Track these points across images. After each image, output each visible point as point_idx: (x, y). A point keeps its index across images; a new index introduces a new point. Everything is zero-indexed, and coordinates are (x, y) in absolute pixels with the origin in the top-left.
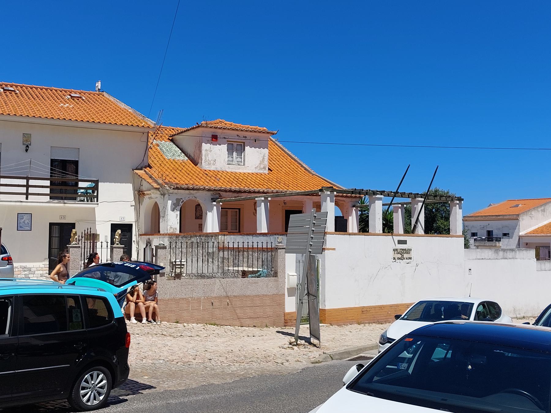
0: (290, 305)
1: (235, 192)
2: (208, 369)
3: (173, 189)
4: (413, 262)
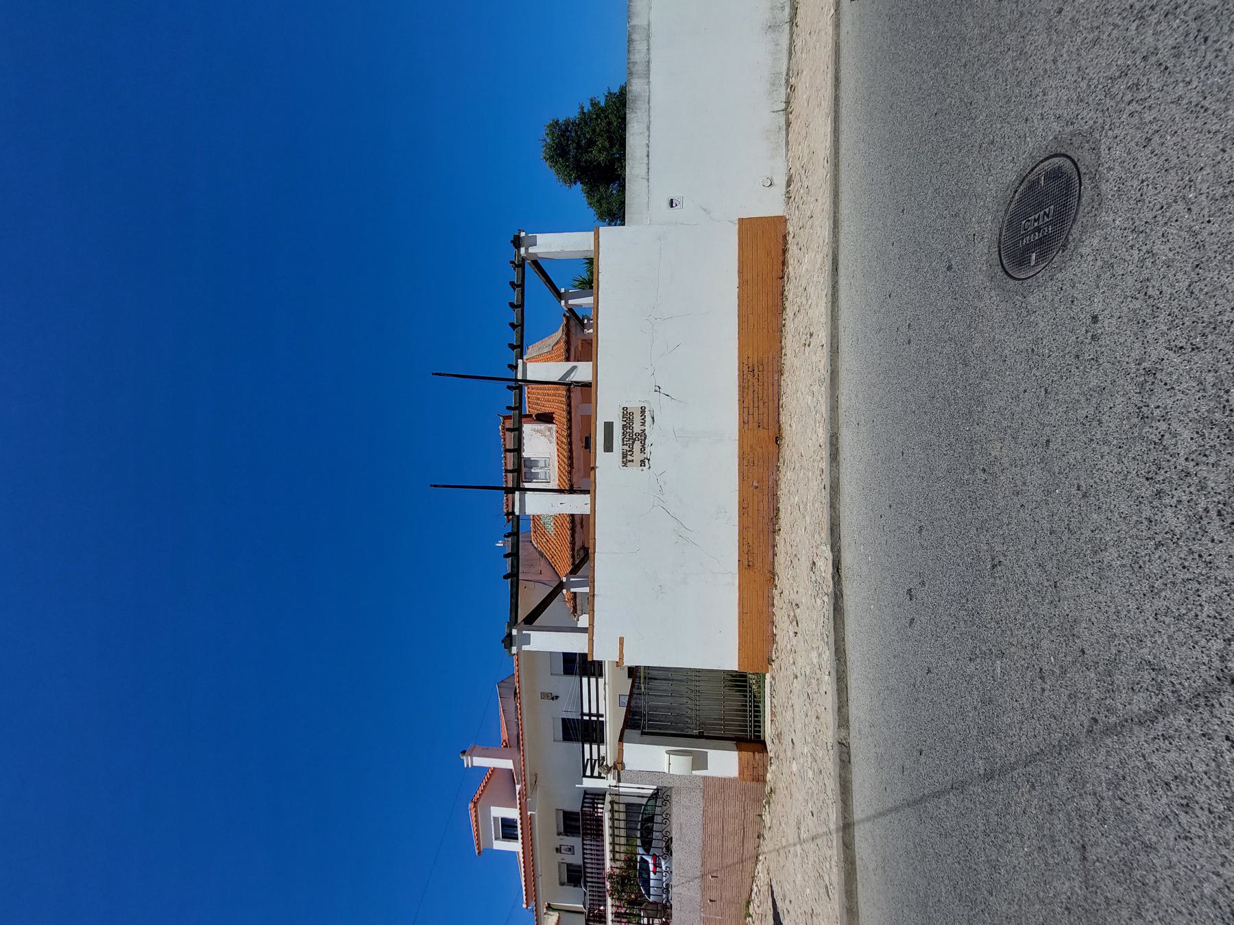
4: (653, 402)
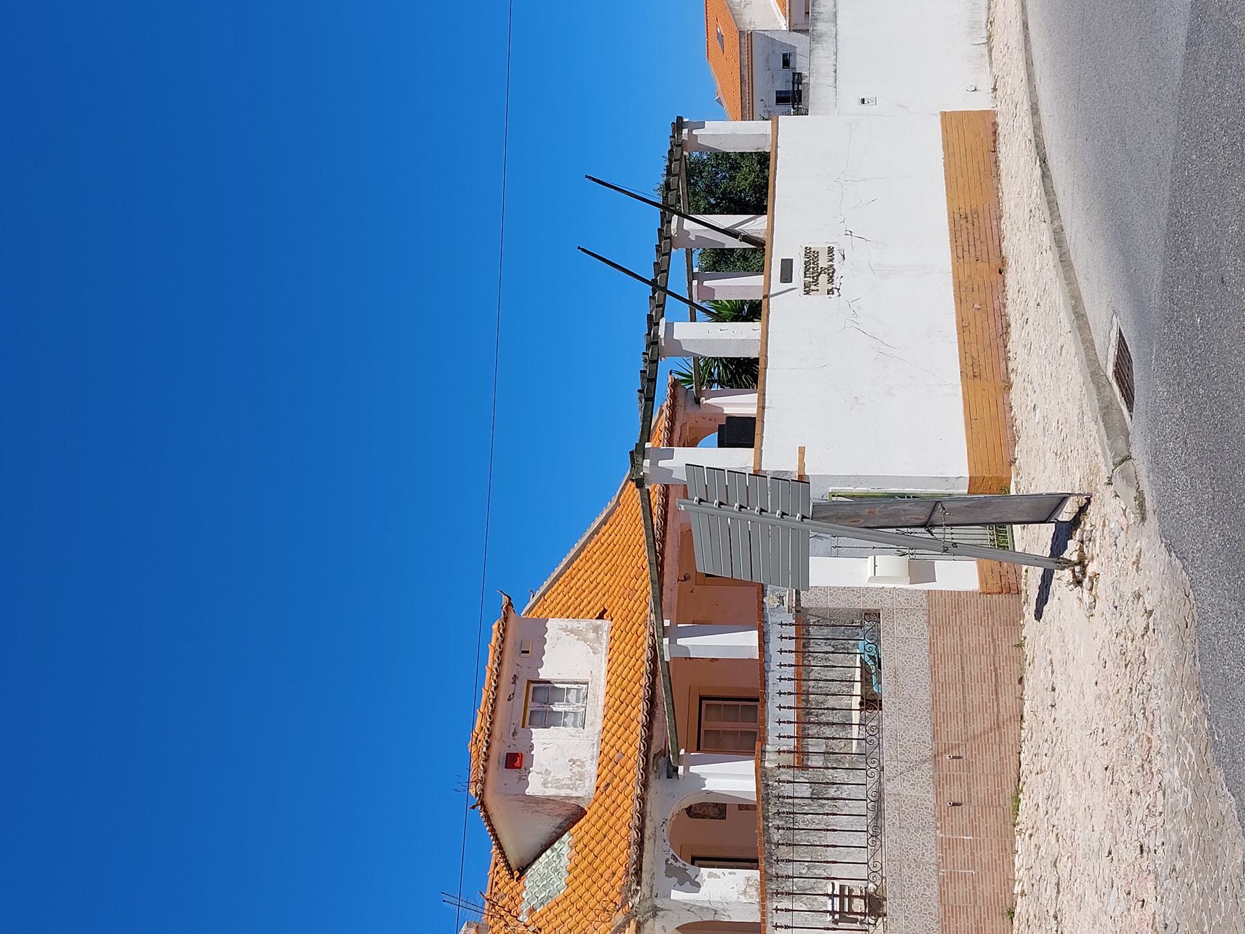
0: (958, 575)
1: (651, 713)
2: (1179, 865)
3: (639, 883)
4: (841, 243)
